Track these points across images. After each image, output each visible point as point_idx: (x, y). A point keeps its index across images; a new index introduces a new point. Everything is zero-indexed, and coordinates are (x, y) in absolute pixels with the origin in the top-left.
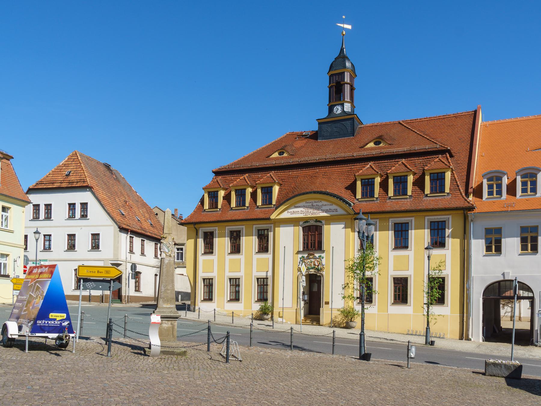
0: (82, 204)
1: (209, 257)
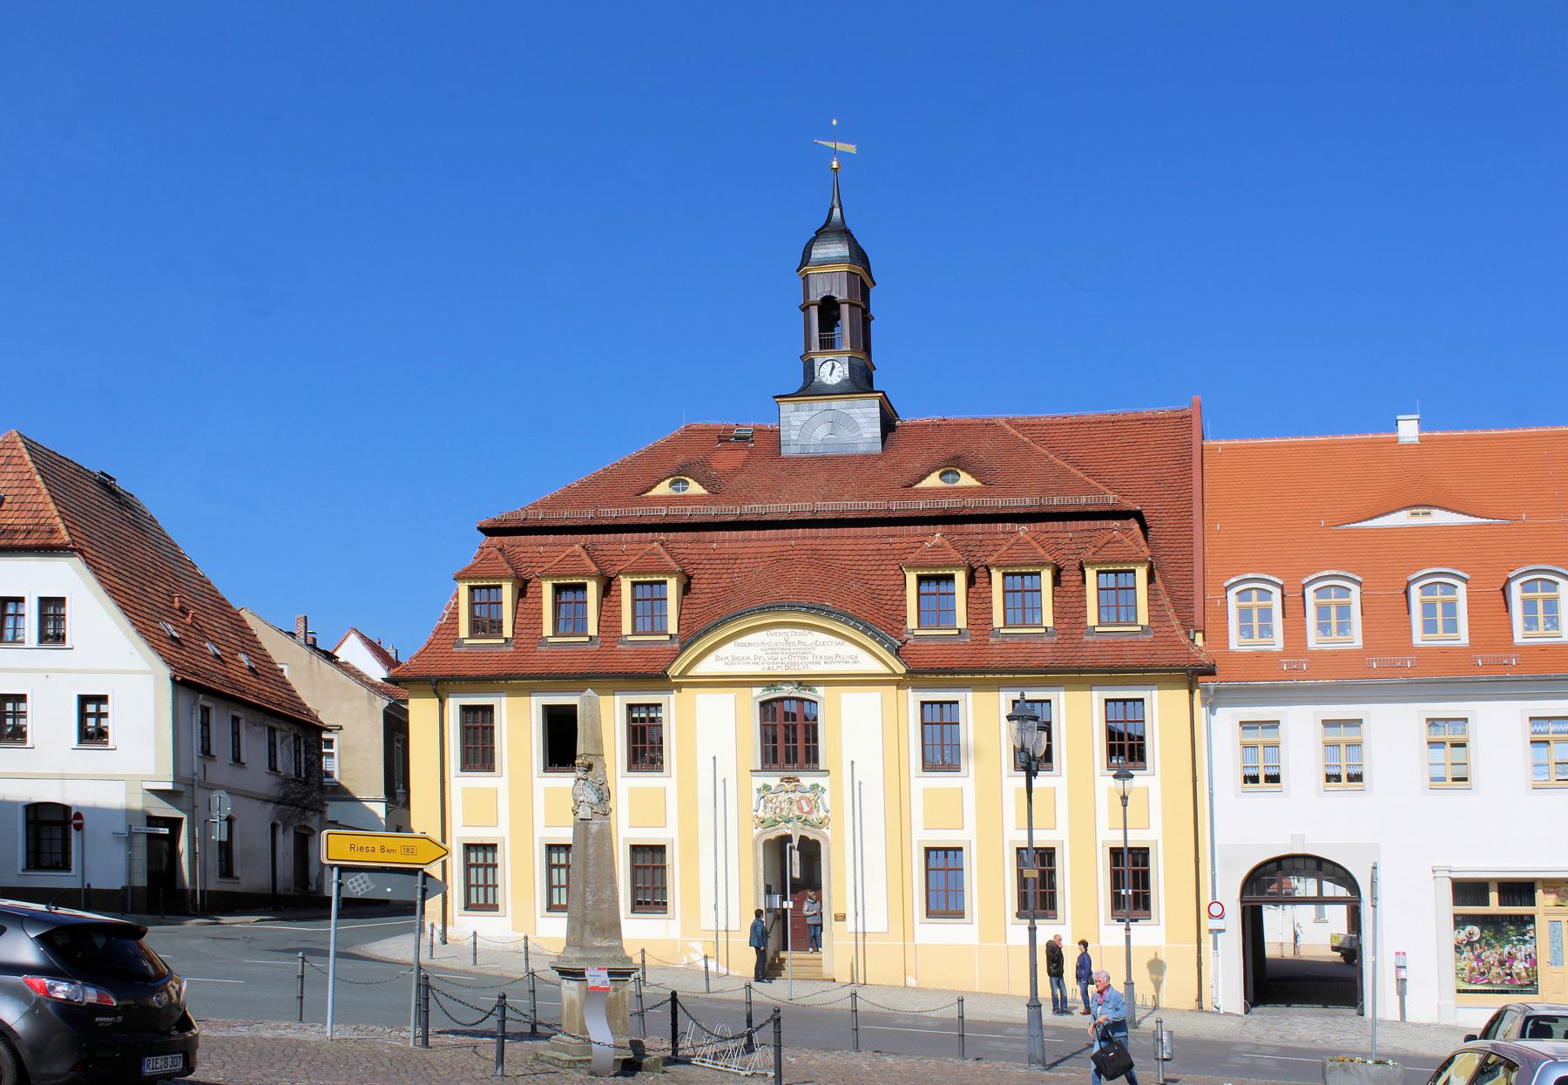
0: (44, 602)
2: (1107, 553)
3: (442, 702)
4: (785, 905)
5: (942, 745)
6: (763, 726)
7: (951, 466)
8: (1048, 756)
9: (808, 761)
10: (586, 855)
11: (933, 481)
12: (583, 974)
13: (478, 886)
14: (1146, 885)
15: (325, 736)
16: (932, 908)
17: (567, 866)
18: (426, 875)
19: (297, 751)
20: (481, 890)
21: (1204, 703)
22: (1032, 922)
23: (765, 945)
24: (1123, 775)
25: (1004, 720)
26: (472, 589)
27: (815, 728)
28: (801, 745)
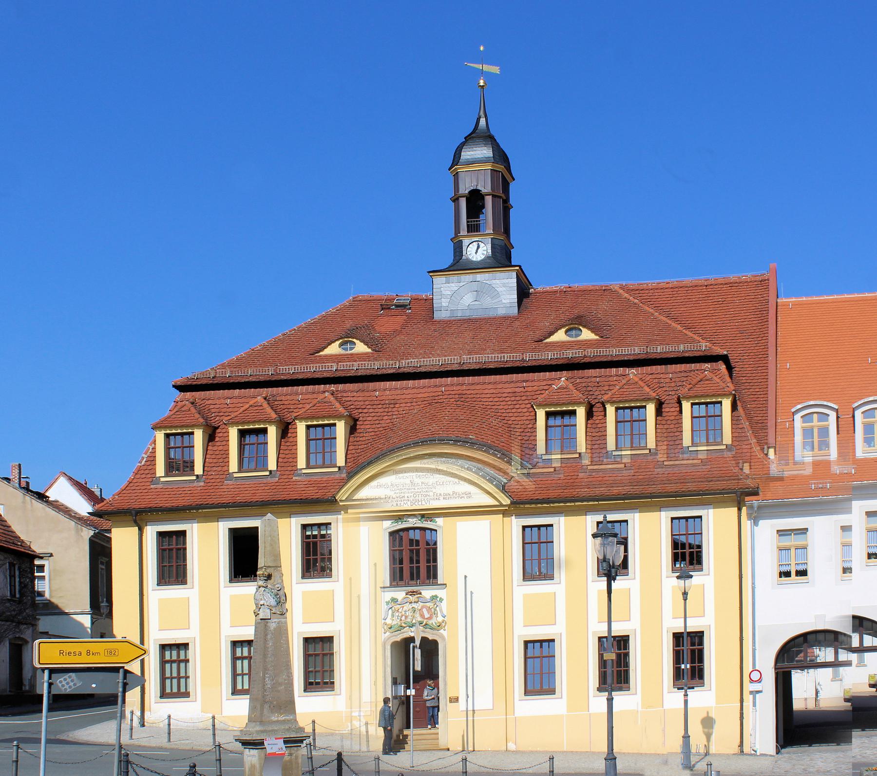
1: (173, 592)
2: (699, 389)
3: (141, 530)
4: (408, 692)
5: (540, 559)
6: (392, 552)
7: (575, 323)
8: (625, 564)
9: (429, 578)
10: (265, 648)
11: (560, 336)
12: (263, 744)
13: (172, 678)
14: (701, 660)
15: (37, 562)
16: (529, 688)
17: (249, 658)
18: (126, 672)
19: (12, 576)
20: (175, 681)
21: (749, 517)
22: (610, 694)
23: (392, 725)
24: (684, 576)
25: (590, 537)
26: (167, 436)
27: (435, 551)
28: (423, 565)
